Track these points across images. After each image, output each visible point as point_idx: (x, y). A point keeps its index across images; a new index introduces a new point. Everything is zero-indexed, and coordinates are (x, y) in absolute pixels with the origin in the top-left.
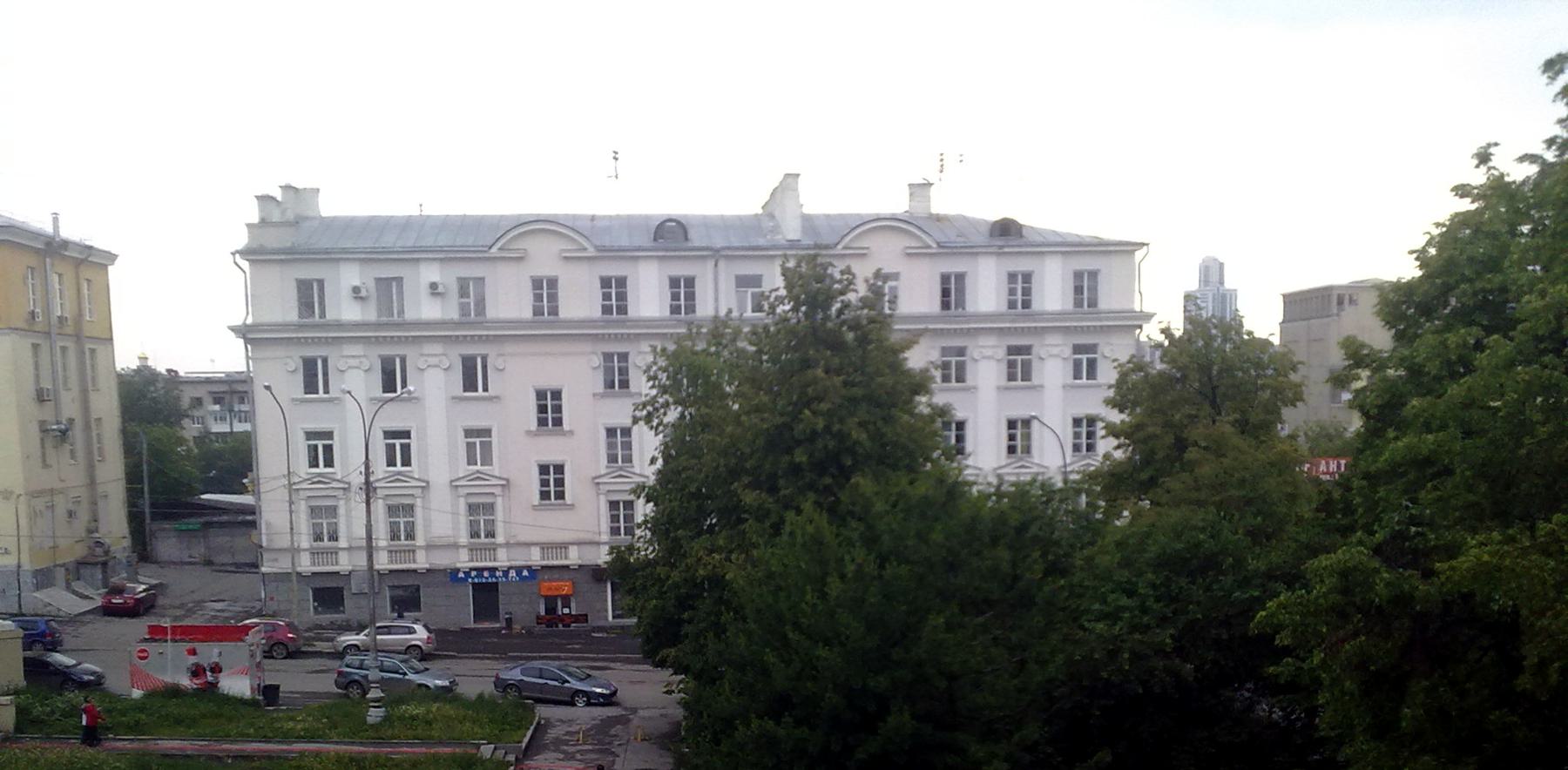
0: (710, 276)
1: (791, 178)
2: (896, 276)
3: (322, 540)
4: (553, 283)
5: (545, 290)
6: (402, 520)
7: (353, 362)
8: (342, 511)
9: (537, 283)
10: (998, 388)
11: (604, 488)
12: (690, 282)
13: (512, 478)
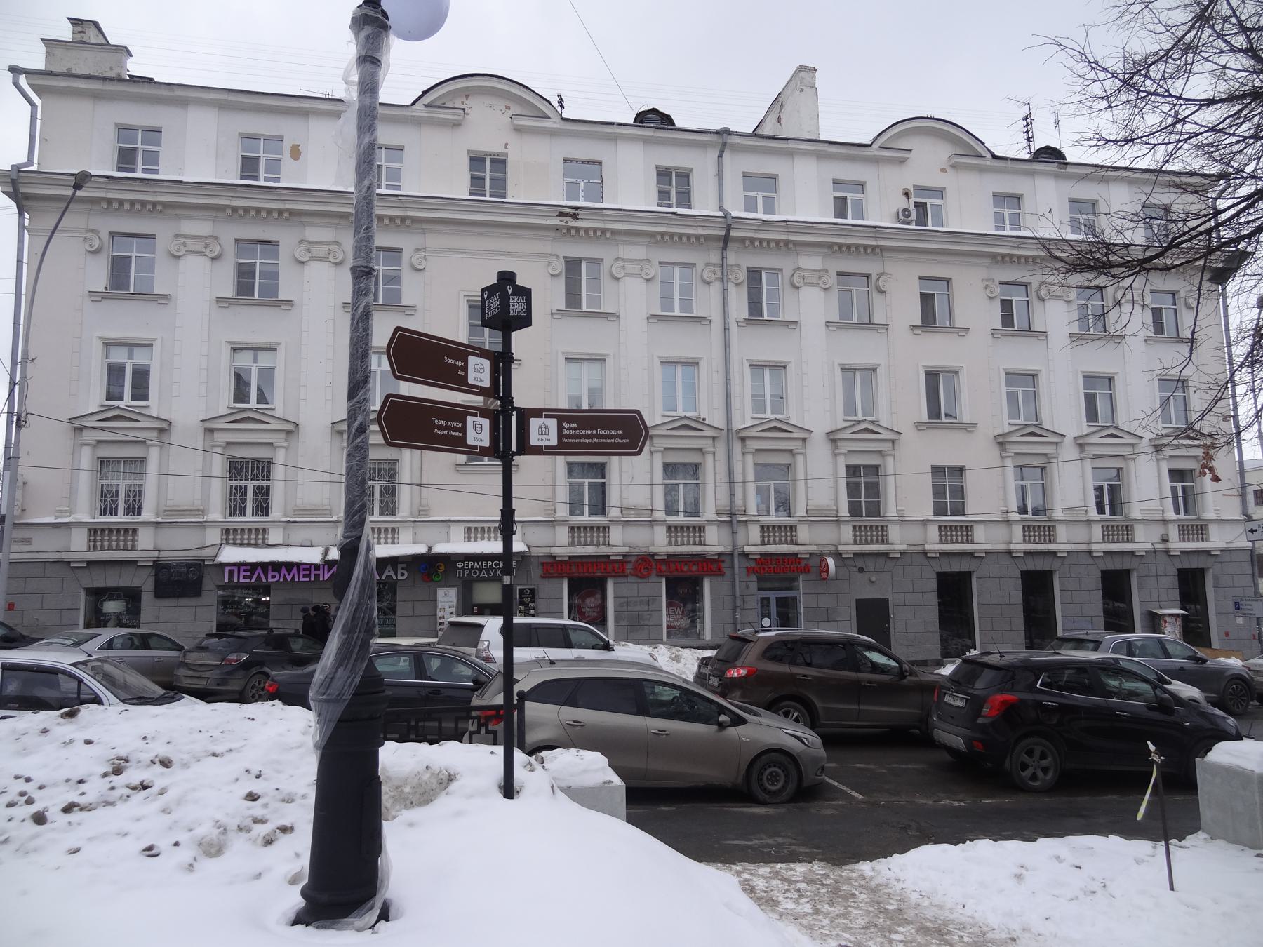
0: (712, 170)
1: (804, 76)
2: (940, 192)
3: (114, 512)
4: (500, 162)
5: (488, 170)
6: (251, 485)
7: (631, 268)
8: (152, 466)
9: (476, 161)
10: (828, 324)
11: (221, 438)
12: (685, 176)
13: (301, 421)
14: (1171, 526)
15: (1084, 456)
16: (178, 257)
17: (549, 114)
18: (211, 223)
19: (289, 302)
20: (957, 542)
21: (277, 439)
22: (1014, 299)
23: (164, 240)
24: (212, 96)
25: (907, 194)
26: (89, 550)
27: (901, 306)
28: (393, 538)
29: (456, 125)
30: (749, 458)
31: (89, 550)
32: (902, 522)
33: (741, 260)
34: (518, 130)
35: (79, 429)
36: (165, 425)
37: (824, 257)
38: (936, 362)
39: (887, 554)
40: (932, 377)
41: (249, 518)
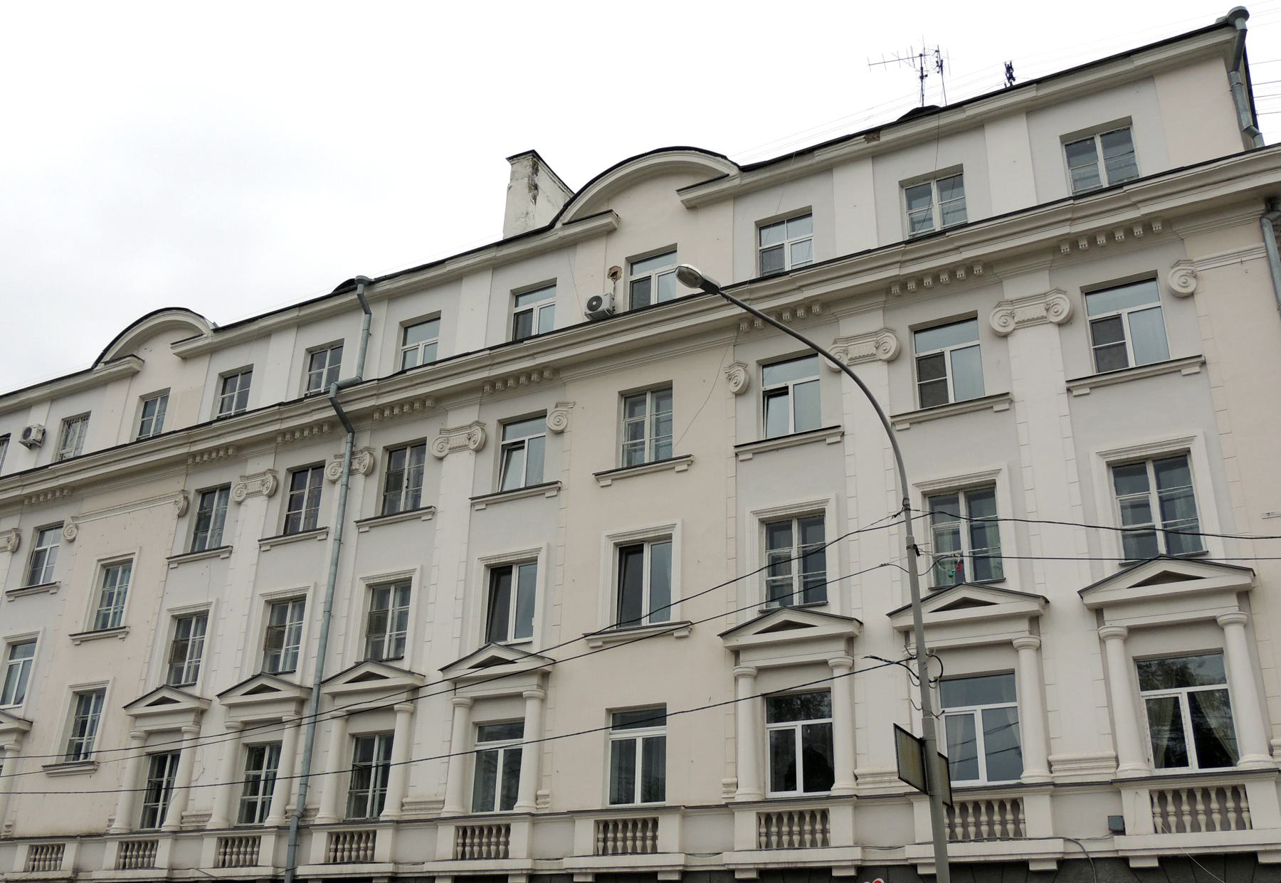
14: (1127, 795)
15: (1103, 631)
16: (1005, 336)
17: (726, 171)
18: (1045, 275)
19: (687, 459)
20: (992, 837)
21: (528, 686)
22: (1124, 313)
23: (992, 318)
24: (1140, 61)
25: (614, 275)
26: (760, 848)
27: (252, 519)
28: (1239, 810)
29: (610, 231)
30: (1114, 647)
31: (760, 848)
32: (1055, 789)
33: (375, 443)
34: (692, 207)
35: (736, 652)
36: (24, 727)
37: (885, 310)
38: (633, 526)
39: (1253, 856)
40: (629, 552)
41: (799, 792)
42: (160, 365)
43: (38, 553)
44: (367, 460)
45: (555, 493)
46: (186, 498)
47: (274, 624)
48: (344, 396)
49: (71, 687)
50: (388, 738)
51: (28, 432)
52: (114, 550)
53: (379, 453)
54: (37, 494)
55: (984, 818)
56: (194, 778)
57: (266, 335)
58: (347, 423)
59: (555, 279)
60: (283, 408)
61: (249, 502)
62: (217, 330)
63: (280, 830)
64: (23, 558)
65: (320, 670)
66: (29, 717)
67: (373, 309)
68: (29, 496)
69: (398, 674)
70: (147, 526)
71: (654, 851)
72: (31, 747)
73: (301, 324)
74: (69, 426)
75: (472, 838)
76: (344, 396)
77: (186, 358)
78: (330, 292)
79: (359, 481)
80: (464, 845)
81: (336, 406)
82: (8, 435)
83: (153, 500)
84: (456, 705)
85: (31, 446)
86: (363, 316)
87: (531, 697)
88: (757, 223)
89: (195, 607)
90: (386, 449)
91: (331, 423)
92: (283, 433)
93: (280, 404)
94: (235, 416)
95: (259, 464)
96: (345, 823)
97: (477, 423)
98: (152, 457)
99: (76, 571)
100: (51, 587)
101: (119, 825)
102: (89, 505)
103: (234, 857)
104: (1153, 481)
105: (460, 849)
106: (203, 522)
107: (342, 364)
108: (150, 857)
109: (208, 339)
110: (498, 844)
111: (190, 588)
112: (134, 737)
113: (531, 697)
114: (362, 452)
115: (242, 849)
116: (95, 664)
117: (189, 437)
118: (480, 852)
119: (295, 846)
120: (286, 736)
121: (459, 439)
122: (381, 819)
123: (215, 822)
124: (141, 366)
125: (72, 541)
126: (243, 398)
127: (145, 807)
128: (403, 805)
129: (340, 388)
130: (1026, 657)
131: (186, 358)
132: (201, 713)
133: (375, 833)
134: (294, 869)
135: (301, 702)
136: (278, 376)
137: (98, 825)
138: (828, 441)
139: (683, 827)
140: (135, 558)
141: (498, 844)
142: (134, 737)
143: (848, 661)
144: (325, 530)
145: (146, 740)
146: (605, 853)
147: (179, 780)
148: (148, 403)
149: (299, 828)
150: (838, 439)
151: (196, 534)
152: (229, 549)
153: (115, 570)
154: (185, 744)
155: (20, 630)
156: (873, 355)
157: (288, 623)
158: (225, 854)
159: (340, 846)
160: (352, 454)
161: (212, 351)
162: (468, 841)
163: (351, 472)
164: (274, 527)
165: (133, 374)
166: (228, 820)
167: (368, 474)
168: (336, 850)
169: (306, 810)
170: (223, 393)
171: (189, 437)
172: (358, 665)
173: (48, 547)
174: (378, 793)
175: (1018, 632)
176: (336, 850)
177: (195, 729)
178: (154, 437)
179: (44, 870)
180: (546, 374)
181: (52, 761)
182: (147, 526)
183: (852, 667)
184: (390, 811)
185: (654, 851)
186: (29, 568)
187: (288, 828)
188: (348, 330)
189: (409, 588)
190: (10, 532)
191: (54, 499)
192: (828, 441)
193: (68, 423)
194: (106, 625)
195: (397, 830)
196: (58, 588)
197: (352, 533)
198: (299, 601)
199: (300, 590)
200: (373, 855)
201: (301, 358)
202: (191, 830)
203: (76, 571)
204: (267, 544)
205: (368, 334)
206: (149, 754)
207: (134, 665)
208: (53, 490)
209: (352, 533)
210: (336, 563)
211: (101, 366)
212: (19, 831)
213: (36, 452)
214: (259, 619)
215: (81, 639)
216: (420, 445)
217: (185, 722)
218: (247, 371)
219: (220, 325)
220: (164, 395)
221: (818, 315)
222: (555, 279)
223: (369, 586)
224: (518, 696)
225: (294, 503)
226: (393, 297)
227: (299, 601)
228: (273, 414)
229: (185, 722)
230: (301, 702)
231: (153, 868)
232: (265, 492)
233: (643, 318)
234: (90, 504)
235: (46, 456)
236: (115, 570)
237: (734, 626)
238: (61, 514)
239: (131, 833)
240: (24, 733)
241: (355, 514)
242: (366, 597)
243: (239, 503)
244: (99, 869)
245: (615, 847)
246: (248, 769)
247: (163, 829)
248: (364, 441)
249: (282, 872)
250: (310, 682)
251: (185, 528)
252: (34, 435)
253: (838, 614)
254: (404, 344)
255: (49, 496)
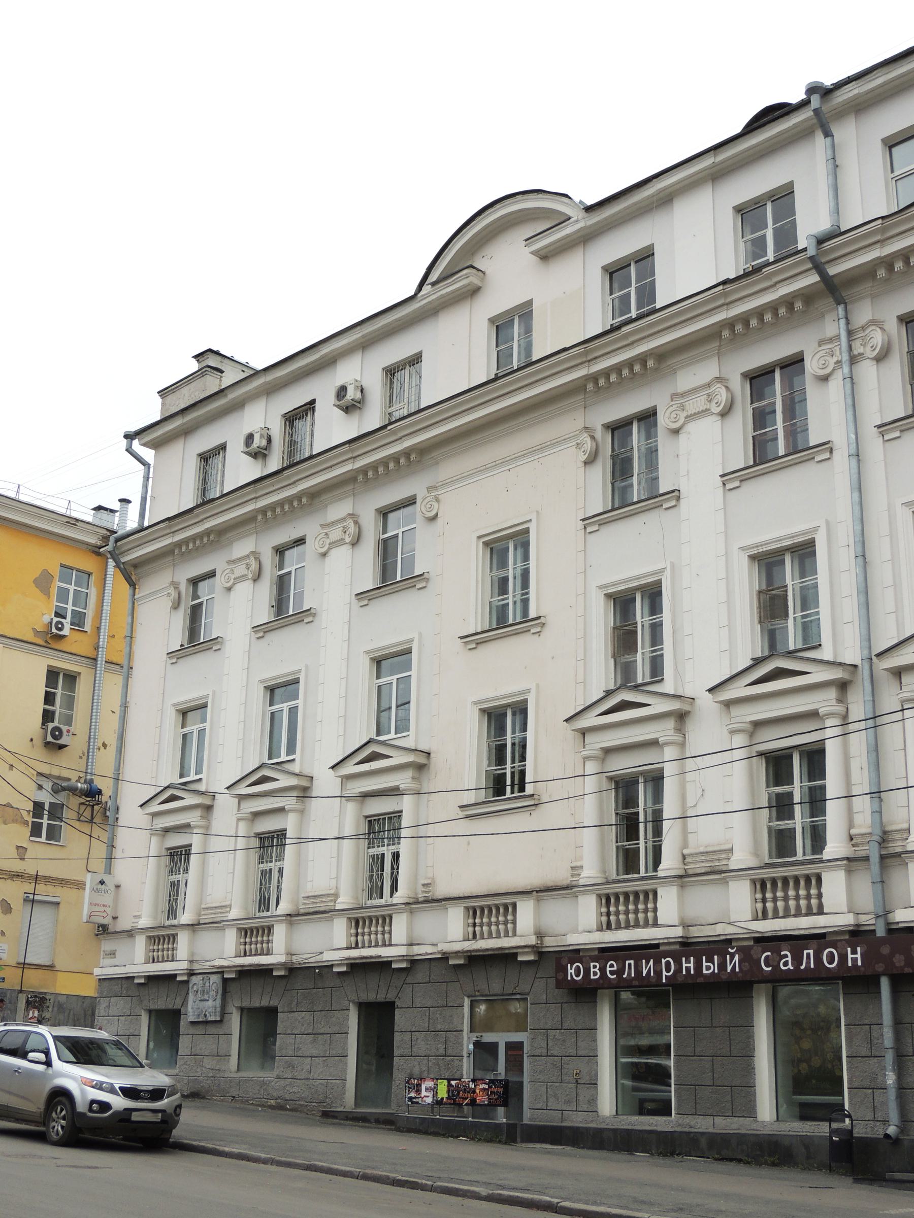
18: (715, 361)
32: (683, 879)
36: (422, 760)
42: (511, 275)
43: (385, 541)
44: (878, 338)
45: (827, 455)
46: (593, 438)
47: (618, 624)
48: (828, 252)
49: (475, 703)
50: (656, 779)
51: (342, 391)
52: (501, 519)
53: (892, 325)
54: (374, 466)
55: (791, 893)
56: (690, 802)
57: (666, 200)
58: (836, 290)
59: (791, 184)
60: (729, 287)
61: (692, 427)
62: (589, 209)
63: (852, 863)
64: (368, 553)
65: (868, 639)
66: (306, 772)
67: (835, 129)
68: (364, 471)
69: (401, 752)
70: (547, 481)
71: (821, 912)
72: (437, 780)
73: (716, 176)
74: (393, 375)
75: (617, 905)
76: (828, 252)
77: (545, 256)
78: (738, 129)
79: (868, 371)
80: (608, 914)
81: (818, 267)
82: (313, 402)
83: (541, 448)
84: (239, 820)
85: (349, 409)
86: (820, 140)
87: (667, 744)
88: (884, 141)
89: (638, 578)
90: (745, 375)
91: (808, 297)
92: (730, 324)
93: (724, 283)
94: (640, 317)
95: (696, 374)
96: (767, 866)
97: (719, 379)
98: (523, 392)
99: (450, 555)
100: (415, 581)
101: (590, 873)
102: (448, 469)
103: (366, 938)
104: (780, 576)
105: (604, 919)
106: (621, 468)
107: (533, 333)
108: (268, 942)
109: (579, 222)
110: (383, 933)
111: (628, 554)
112: (585, 759)
113: (667, 744)
114: (863, 328)
115: (493, 919)
116: (505, 670)
117: (586, 353)
118: (787, 908)
119: (882, 882)
120: (406, 804)
121: (336, 534)
122: (660, 874)
123: (741, 858)
124: (482, 280)
125: (434, 518)
126: (648, 293)
127: (617, 847)
128: (684, 857)
129: (117, 540)
130: (669, 753)
131: (545, 256)
132: (681, 717)
133: (514, 906)
134: (887, 913)
135: (843, 686)
136: (696, 252)
137: (562, 876)
138: (665, 506)
139: (680, 898)
140: (533, 528)
141: (646, 911)
142: (733, 732)
143: (840, 709)
144: (826, 446)
145: (603, 760)
146: (765, 916)
147: (669, 808)
148: (501, 326)
149: (882, 858)
150: (827, 455)
151: (613, 484)
152: (675, 494)
153: (506, 550)
154: (829, 733)
155: (188, 695)
156: (707, 410)
157: (638, 618)
158: (357, 935)
159: (360, 930)
160: (850, 333)
161: (585, 238)
162: (612, 909)
163: (854, 360)
164: (739, 454)
165: (473, 292)
166: (604, 872)
167: (881, 358)
168: (474, 925)
169: (885, 833)
170: (611, 294)
171: (586, 353)
172: (609, 693)
173: (293, 569)
174: (650, 844)
175: (664, 731)
176: (474, 925)
177: (840, 709)
178: (519, 369)
179: (490, 936)
180: (650, 363)
181: (469, 798)
182: (547, 481)
183: (845, 716)
184: (669, 863)
185: (821, 912)
186: (379, 561)
187: (866, 859)
188: (802, 169)
189: (659, 593)
190: (344, 519)
191: (275, 517)
192: (817, 459)
193: (391, 372)
194: (508, 615)
195: (291, 924)
196: (427, 580)
197: (874, 446)
198: (804, 551)
199: (201, 698)
200: (656, 918)
201: (729, 222)
202: (711, 871)
203: (450, 555)
204: (733, 479)
205: (835, 166)
206: (761, 754)
207: (561, 666)
208: (395, 458)
209: (874, 446)
210: (859, 487)
211: (427, 289)
212: (441, 890)
213: (355, 417)
214: (745, 583)
215: (474, 640)
216: (648, 417)
217: (193, 817)
218: (645, 257)
219: (590, 202)
220: (524, 312)
221: (656, 370)
222: (791, 184)
223: (752, 558)
224: (281, 810)
225: (761, 418)
226: (861, 107)
227: (804, 551)
228: (714, 299)
229: (193, 817)
230: (843, 686)
231: (390, 945)
232: (348, 540)
233: (511, 383)
234: (449, 468)
235: (372, 419)
236: (506, 550)
237: (895, 641)
238: (308, 527)
239: (608, 883)
240: (420, 768)
241: (872, 416)
242: (264, 697)
243: (676, 432)
244: (575, 931)
245: (776, 909)
246: (768, 786)
247: (660, 874)
248: (863, 313)
249: (867, 920)
250: (852, 654)
251: (600, 475)
252: (351, 394)
253: (672, 692)
254: (892, 171)
255: (286, 507)
